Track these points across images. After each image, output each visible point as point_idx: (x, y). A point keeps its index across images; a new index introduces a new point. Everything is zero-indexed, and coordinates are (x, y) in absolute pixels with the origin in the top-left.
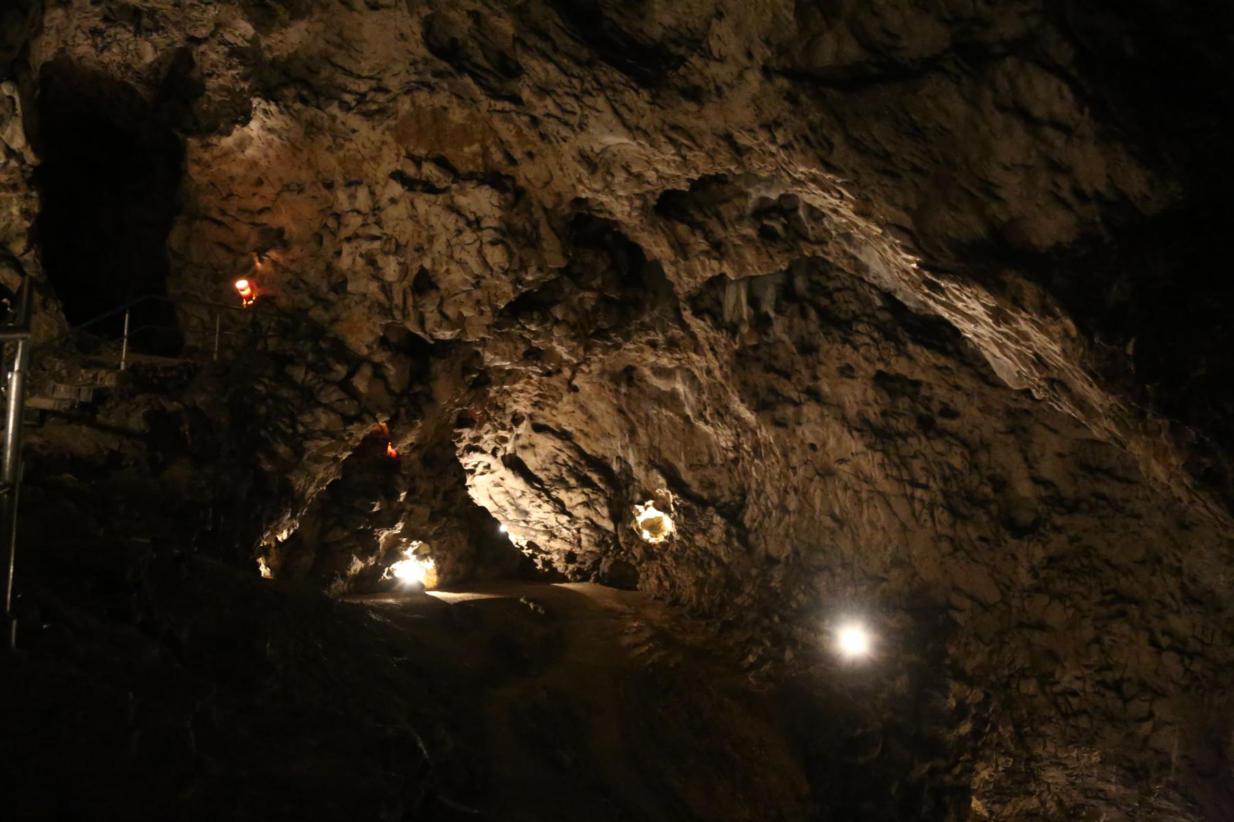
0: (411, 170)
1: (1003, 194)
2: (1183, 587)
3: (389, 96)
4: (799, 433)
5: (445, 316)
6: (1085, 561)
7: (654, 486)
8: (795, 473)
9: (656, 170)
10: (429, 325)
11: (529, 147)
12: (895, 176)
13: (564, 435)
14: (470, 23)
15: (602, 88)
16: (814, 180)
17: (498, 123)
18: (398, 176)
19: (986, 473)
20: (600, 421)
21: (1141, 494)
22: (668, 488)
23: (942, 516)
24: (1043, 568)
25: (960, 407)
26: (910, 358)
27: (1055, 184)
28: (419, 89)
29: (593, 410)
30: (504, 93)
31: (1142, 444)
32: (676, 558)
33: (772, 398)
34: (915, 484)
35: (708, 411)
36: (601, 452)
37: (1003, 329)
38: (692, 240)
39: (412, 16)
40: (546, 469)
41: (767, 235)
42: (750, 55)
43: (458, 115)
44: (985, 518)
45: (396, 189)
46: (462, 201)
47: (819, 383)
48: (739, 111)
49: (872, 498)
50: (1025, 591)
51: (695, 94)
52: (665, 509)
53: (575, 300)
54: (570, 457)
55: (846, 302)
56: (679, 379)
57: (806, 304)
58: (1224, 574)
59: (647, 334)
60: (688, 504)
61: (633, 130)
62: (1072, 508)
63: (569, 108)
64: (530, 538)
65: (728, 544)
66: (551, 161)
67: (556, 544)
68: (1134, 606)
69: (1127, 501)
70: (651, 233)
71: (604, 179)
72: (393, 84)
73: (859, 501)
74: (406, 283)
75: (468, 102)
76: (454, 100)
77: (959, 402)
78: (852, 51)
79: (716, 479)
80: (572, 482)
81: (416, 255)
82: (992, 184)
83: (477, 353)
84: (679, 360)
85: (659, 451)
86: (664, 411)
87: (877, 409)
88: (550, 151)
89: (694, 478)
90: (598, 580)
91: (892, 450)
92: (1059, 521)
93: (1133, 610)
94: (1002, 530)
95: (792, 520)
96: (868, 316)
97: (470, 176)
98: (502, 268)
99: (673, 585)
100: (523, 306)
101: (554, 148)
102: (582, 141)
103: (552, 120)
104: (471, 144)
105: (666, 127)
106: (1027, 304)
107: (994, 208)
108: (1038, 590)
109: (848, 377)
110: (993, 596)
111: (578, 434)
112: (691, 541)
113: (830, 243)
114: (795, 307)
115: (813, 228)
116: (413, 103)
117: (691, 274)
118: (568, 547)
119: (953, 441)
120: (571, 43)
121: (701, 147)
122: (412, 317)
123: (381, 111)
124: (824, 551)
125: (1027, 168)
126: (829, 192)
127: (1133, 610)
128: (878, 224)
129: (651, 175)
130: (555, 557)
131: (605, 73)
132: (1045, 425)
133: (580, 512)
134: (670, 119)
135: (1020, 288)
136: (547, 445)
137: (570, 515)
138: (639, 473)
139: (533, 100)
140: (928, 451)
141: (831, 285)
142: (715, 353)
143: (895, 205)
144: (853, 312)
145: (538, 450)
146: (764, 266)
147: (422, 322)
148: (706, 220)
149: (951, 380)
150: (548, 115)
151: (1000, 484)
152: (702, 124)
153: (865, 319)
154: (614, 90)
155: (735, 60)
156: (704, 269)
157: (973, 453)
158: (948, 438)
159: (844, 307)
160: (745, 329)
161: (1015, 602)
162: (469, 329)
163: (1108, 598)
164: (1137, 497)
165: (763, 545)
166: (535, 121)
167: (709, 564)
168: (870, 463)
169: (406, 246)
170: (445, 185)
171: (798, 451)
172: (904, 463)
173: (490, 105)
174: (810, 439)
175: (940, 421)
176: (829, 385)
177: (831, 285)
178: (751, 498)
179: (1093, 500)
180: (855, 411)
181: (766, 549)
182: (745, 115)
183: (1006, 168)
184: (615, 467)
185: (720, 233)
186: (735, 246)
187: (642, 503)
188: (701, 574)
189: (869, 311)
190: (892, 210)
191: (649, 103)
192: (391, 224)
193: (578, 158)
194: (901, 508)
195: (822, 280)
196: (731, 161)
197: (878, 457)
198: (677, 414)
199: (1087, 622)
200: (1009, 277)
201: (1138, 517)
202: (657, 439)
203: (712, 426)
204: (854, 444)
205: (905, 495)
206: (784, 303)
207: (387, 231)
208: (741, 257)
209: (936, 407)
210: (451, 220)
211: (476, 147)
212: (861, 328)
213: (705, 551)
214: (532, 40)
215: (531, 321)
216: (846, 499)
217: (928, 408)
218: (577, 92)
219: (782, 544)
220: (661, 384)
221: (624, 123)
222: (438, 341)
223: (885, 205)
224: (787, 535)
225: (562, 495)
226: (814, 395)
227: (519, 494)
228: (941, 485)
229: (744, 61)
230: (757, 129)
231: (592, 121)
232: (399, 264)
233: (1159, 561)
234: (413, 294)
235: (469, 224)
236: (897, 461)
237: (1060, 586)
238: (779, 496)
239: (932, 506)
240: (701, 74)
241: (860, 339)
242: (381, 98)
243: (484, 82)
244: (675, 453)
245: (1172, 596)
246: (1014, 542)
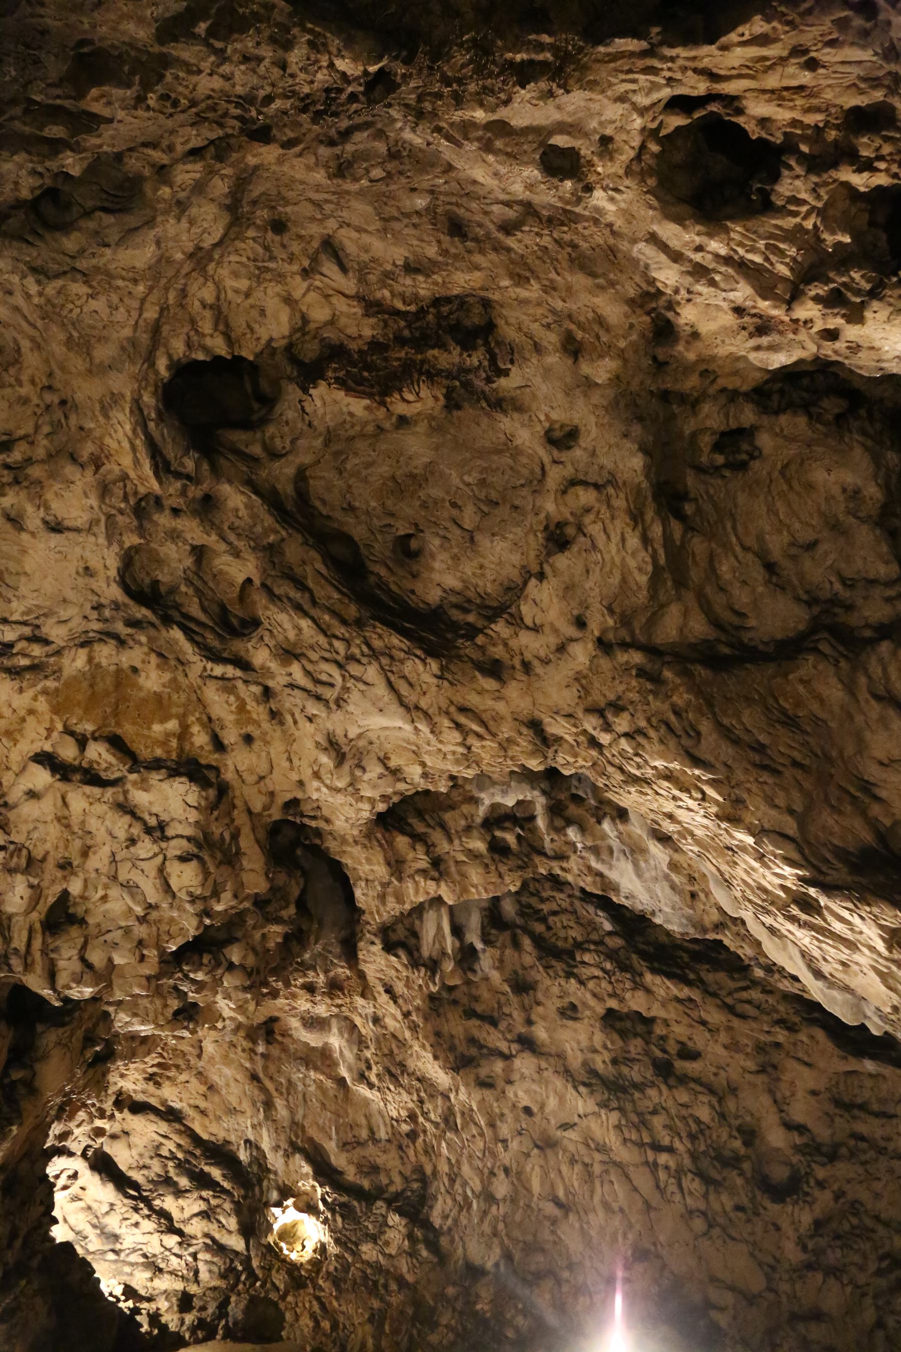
0: (68, 752)
1: (883, 794)
3: (50, 649)
4: (511, 1095)
5: (89, 966)
6: (855, 1221)
7: (294, 1177)
8: (506, 1148)
9: (423, 764)
10: (62, 979)
11: (250, 729)
12: (775, 772)
13: (171, 1115)
14: (189, 562)
15: (375, 654)
16: (668, 776)
17: (212, 694)
18: (45, 759)
20: (224, 1092)
22: (315, 1179)
23: (693, 1184)
24: (811, 1237)
26: (648, 991)
28: (100, 640)
29: (215, 1078)
30: (225, 655)
32: (336, 1282)
33: (474, 1051)
34: (657, 1148)
35: (375, 1069)
36: (222, 1135)
38: (411, 855)
39: (110, 544)
40: (145, 1167)
41: (498, 849)
42: (580, 623)
43: (153, 680)
44: (739, 1181)
45: (41, 777)
46: (139, 797)
47: (533, 1028)
48: (555, 690)
49: (607, 1172)
50: (795, 1271)
51: (495, 669)
52: (309, 1208)
53: (257, 936)
54: (179, 1146)
55: (564, 927)
56: (335, 1030)
59: (305, 975)
60: (344, 1199)
61: (411, 710)
62: (832, 1156)
63: (324, 677)
64: (125, 1278)
65: (412, 1254)
66: (277, 749)
67: (164, 1283)
70: (365, 846)
71: (352, 774)
72: (56, 633)
73: (589, 1176)
74: (35, 916)
75: (173, 663)
76: (154, 659)
77: (699, 1039)
78: (699, 627)
79: (380, 1161)
80: (184, 1182)
81: (59, 874)
82: (867, 782)
83: (106, 1014)
84: (339, 1006)
85: (303, 1127)
86: (312, 1073)
87: (607, 1056)
88: (278, 733)
89: (350, 1162)
90: (229, 1334)
94: (758, 1193)
95: (501, 1211)
96: (596, 943)
97: (156, 765)
98: (190, 894)
99: (335, 1326)
100: (205, 947)
101: (284, 732)
102: (335, 722)
103: (296, 692)
104: (164, 720)
105: (452, 709)
108: (809, 1266)
110: (757, 1283)
111: (191, 1112)
112: (355, 1254)
113: (573, 858)
114: (504, 937)
115: (552, 840)
116: (90, 660)
117: (400, 899)
118: (179, 1286)
119: (698, 1088)
120: (336, 596)
121: (494, 735)
122: (39, 968)
123: (34, 668)
124: (543, 1250)
128: (751, 832)
129: (414, 772)
130: (163, 1304)
131: (380, 637)
132: (798, 1059)
133: (196, 1228)
134: (458, 699)
136: (146, 1130)
137: (180, 1233)
138: (275, 1161)
139: (273, 665)
140: (670, 1104)
142: (394, 998)
143: (777, 807)
144: (574, 939)
145: (133, 1139)
146: (491, 887)
147: (52, 976)
148: (429, 830)
149: (695, 1014)
150: (292, 686)
151: (749, 1135)
152: (501, 707)
153: (592, 947)
154: (392, 658)
155: (556, 631)
156: (417, 892)
157: (721, 1100)
158: (692, 1085)
159: (562, 934)
160: (449, 966)
161: (785, 1287)
162: (116, 982)
163: (884, 1264)
165: (460, 1251)
166: (267, 693)
167: (386, 1286)
168: (604, 1127)
169: (44, 860)
170: (117, 775)
171: (510, 1117)
172: (643, 1123)
173: (205, 669)
174: (525, 1101)
176: (547, 1030)
178: (440, 1186)
180: (580, 1060)
182: (566, 698)
183: (881, 763)
184: (243, 1156)
185: (444, 847)
186: (457, 862)
187: (279, 1204)
188: (376, 1304)
189: (595, 937)
190: (773, 813)
191: (436, 676)
192: (24, 828)
193: (325, 743)
194: (642, 1179)
195: (534, 901)
196: (533, 754)
197: (614, 1117)
198: (329, 1077)
199: (868, 1300)
202: (301, 1112)
203: (379, 1089)
204: (581, 1103)
206: (493, 931)
207: (14, 837)
208: (464, 875)
209: (673, 1048)
210: (121, 825)
211: (172, 725)
212: (587, 958)
213: (377, 1268)
214: (283, 588)
215: (199, 967)
216: (573, 1176)
217: (664, 1051)
218: (339, 658)
220: (312, 1039)
221: (402, 703)
222: (67, 1000)
223: (763, 807)
224: (495, 1234)
225: (169, 1203)
226: (528, 1044)
227: (106, 1208)
228: (689, 1146)
229: (571, 631)
230: (580, 715)
231: (355, 696)
232: (31, 886)
234: (43, 934)
235: (149, 830)
236: (634, 1118)
237: (833, 1256)
238: (482, 1181)
239: (678, 1174)
240: (506, 645)
242: (37, 650)
243: (198, 638)
244: (322, 1129)
246: (777, 1207)
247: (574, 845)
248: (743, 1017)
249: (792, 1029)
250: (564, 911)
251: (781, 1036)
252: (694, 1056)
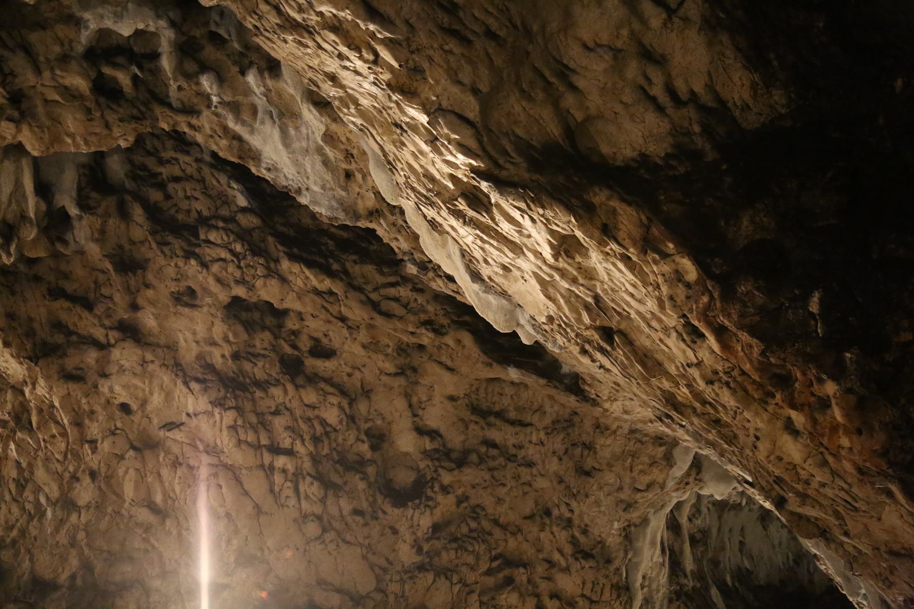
2: (574, 541)
4: (104, 388)
6: (473, 525)
8: (94, 450)
12: (465, 41)
16: (336, 27)
19: (365, 426)
21: (534, 439)
23: (311, 489)
24: (428, 540)
25: (336, 343)
26: (283, 280)
27: (649, 80)
31: (765, 416)
33: (59, 338)
34: (275, 450)
37: (562, 264)
41: (106, 91)
44: (362, 485)
47: (139, 314)
50: (406, 572)
57: (128, 198)
58: (619, 521)
62: (461, 460)
68: (522, 570)
69: (521, 447)
77: (337, 336)
87: (227, 351)
91: (248, 406)
92: (447, 478)
93: (521, 576)
95: (83, 519)
96: (225, 220)
106: (621, 235)
107: (569, 101)
108: (421, 568)
109: (187, 305)
113: (206, 113)
114: (110, 202)
115: (180, 88)
119: (329, 389)
125: (617, 52)
126: (358, 49)
127: (521, 576)
132: (440, 363)
135: (614, 211)
140: (295, 404)
141: (165, 171)
143: (459, 83)
144: (199, 213)
151: (378, 439)
153: (221, 224)
158: (322, 385)
159: (184, 205)
160: (30, 234)
161: (394, 588)
163: (495, 564)
164: (530, 442)
165: (27, 564)
171: (101, 416)
174: (122, 396)
175: (313, 364)
177: (165, 171)
179: (483, 449)
180: (194, 354)
181: (32, 571)
183: (586, 47)
189: (224, 212)
190: (455, 90)
197: (230, 417)
200: (600, 197)
201: (530, 465)
205: (262, 466)
206: (94, 195)
208: (56, 120)
209: (305, 344)
212: (213, 236)
219: (64, 559)
223: (444, 81)
226: (131, 332)
228: (312, 449)
233: (548, 513)
236: (254, 419)
237: (447, 558)
238: (61, 487)
241: (210, 253)
245: (560, 551)
246: (396, 511)
248: (388, 315)
249: (438, 331)
250: (189, 178)
252: (327, 353)
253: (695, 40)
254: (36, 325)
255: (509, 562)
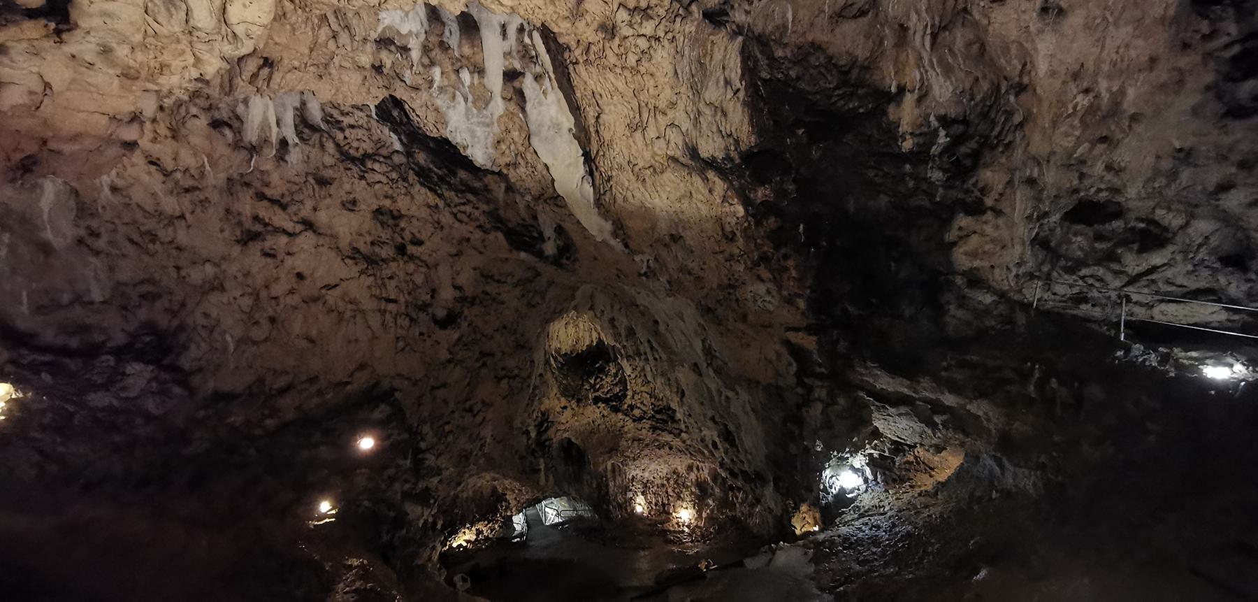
34: (389, 301)
62: (472, 301)
127: (489, 361)
159: (355, 144)
175: (411, 249)
201: (503, 303)
209: (408, 236)
212: (376, 166)
223: (1118, 151)
236: (379, 282)
247: (431, 82)
248: (460, 221)
249: (486, 232)
250: (361, 127)
251: (478, 235)
252: (419, 243)
253: (739, 107)
254: (243, 219)
255: (483, 354)
